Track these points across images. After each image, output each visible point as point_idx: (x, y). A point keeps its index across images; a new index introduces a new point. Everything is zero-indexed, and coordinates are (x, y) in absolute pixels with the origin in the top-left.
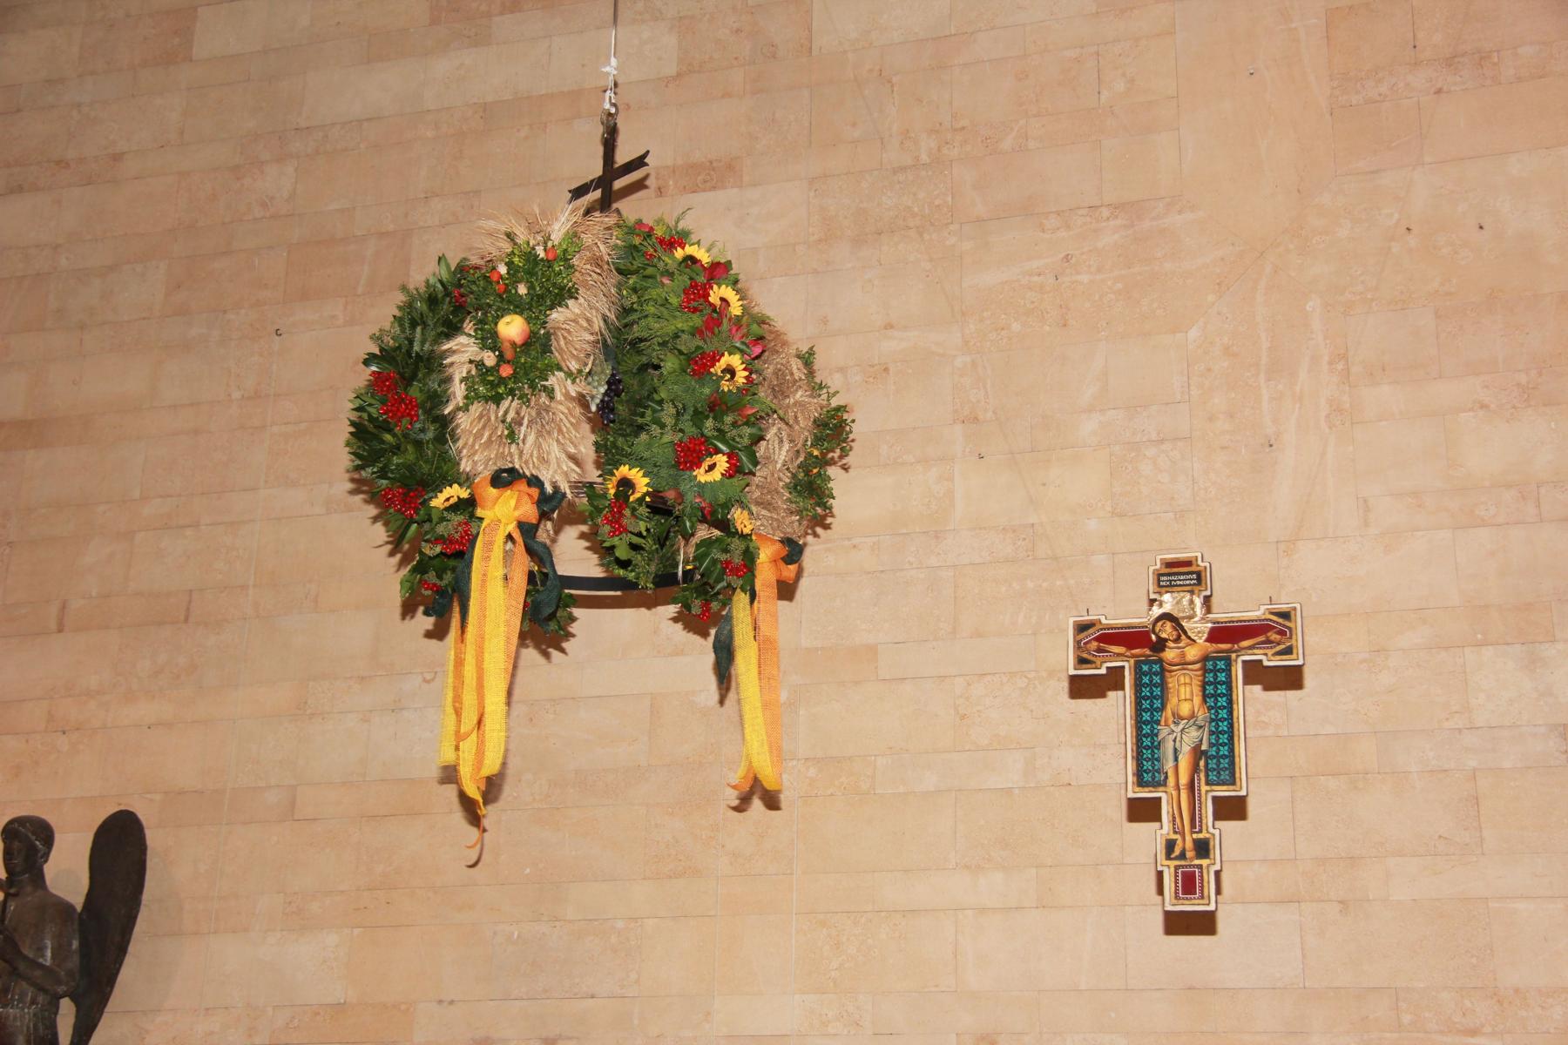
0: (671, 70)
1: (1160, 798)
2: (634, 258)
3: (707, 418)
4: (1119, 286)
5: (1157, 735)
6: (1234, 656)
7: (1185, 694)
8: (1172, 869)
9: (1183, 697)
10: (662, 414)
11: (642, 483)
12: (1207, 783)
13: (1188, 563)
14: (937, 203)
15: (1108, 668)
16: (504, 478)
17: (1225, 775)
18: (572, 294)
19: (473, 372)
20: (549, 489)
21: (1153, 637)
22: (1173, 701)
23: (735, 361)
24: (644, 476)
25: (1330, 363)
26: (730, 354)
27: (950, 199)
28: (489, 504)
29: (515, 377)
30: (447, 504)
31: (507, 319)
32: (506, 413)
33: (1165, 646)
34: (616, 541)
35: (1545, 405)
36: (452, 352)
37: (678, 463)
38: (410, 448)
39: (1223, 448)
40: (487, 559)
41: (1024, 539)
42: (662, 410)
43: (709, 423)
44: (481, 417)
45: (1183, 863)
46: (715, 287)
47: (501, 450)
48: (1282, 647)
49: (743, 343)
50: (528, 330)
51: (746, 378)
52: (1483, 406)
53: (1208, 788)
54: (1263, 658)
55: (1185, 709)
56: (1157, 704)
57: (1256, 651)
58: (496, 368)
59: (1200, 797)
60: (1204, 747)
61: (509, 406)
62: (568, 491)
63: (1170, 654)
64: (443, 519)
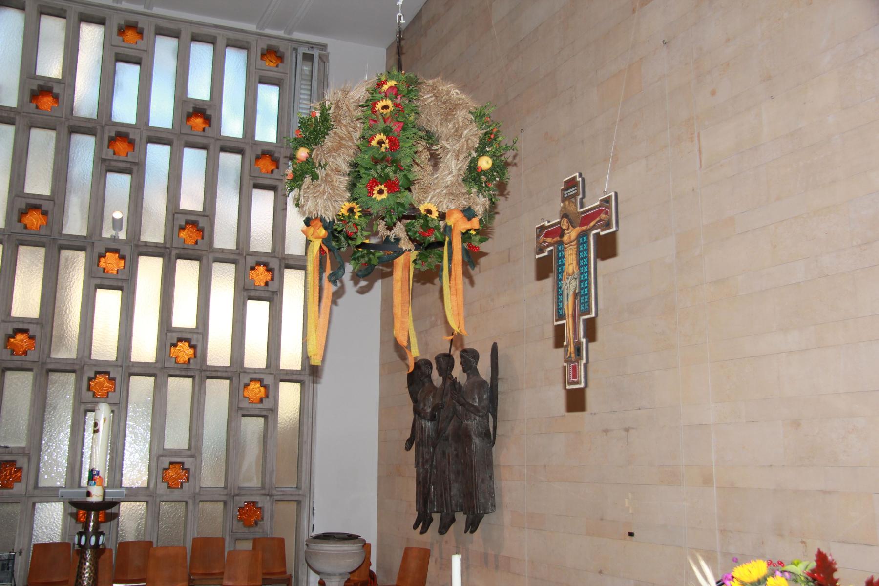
15: (549, 251)
33: (564, 234)
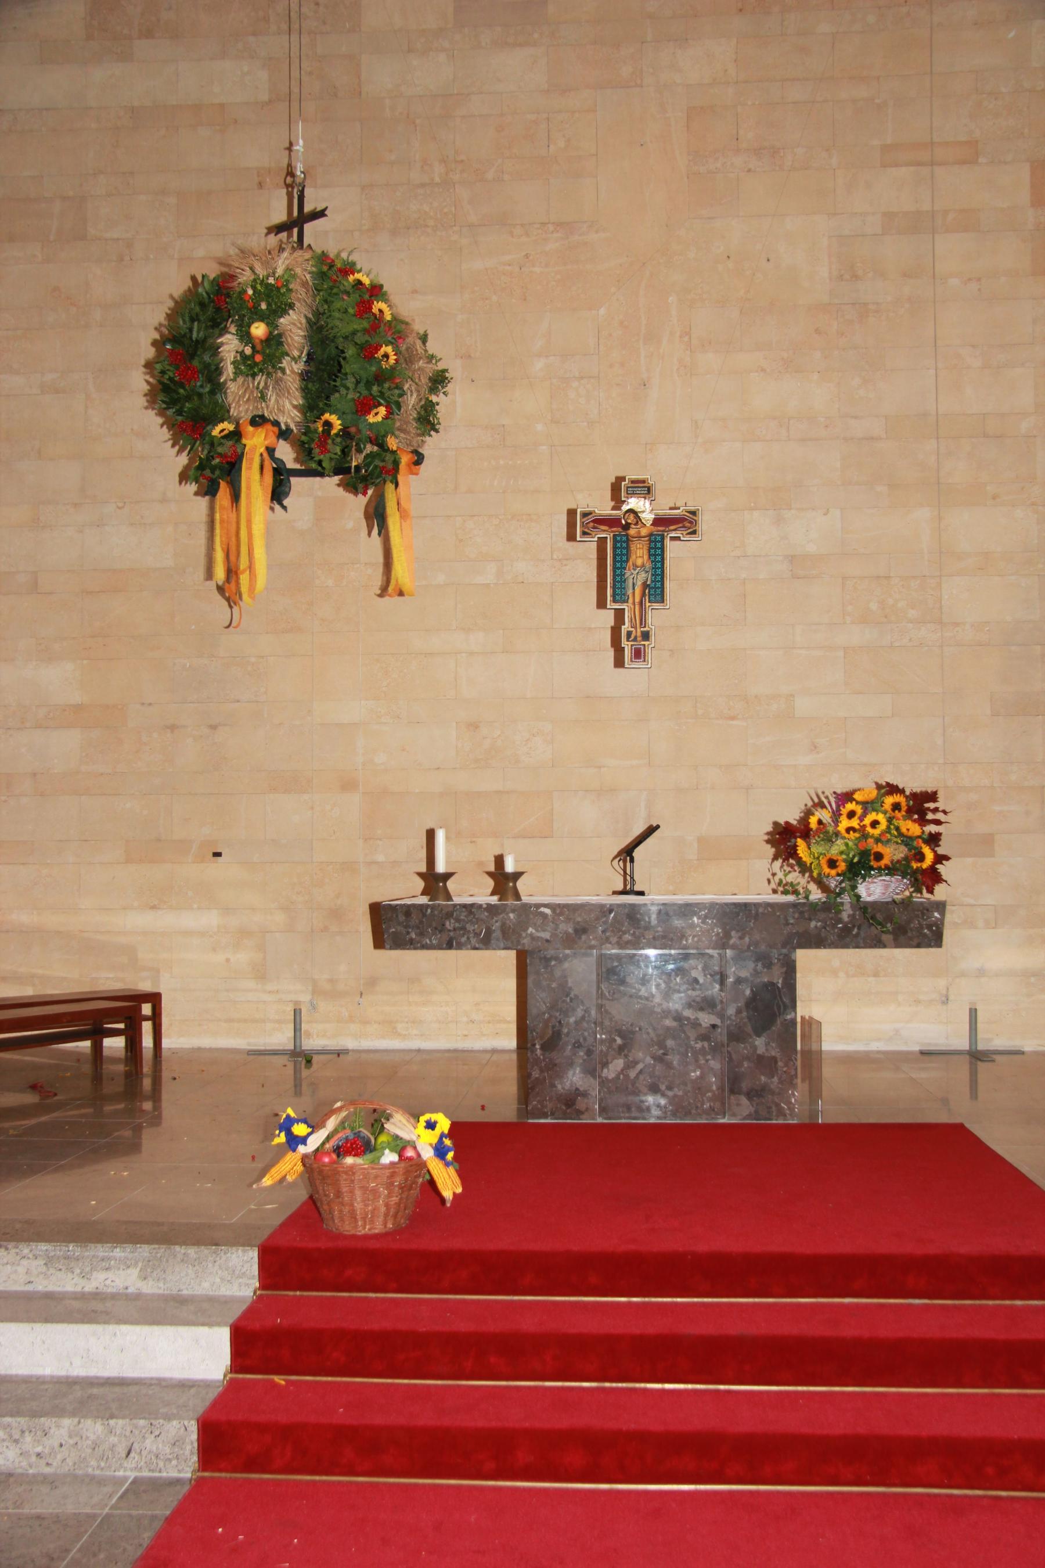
0: (265, 98)
1: (624, 609)
2: (323, 280)
3: (374, 385)
4: (559, 277)
5: (624, 575)
6: (666, 534)
7: (639, 554)
8: (630, 647)
9: (638, 555)
10: (347, 381)
11: (337, 423)
12: (649, 602)
13: (643, 482)
14: (446, 210)
16: (258, 421)
17: (659, 598)
18: (291, 306)
19: (239, 358)
20: (283, 427)
21: (623, 522)
22: (633, 557)
23: (389, 349)
24: (338, 419)
25: (681, 337)
26: (386, 346)
27: (453, 209)
28: (250, 436)
29: (264, 362)
30: (222, 434)
31: (256, 325)
32: (259, 384)
34: (322, 457)
35: (796, 372)
36: (222, 344)
37: (357, 411)
38: (196, 398)
39: (618, 385)
40: (249, 468)
41: (498, 434)
42: (347, 379)
43: (375, 388)
44: (243, 383)
45: (635, 643)
46: (375, 302)
47: (256, 405)
48: (691, 530)
49: (393, 338)
50: (268, 331)
51: (396, 360)
52: (763, 370)
53: (649, 604)
54: (681, 535)
55: (639, 562)
56: (624, 558)
57: (678, 532)
58: (253, 356)
59: (645, 609)
60: (648, 583)
61: (261, 379)
62: (294, 428)
63: (632, 532)
64: (221, 444)
